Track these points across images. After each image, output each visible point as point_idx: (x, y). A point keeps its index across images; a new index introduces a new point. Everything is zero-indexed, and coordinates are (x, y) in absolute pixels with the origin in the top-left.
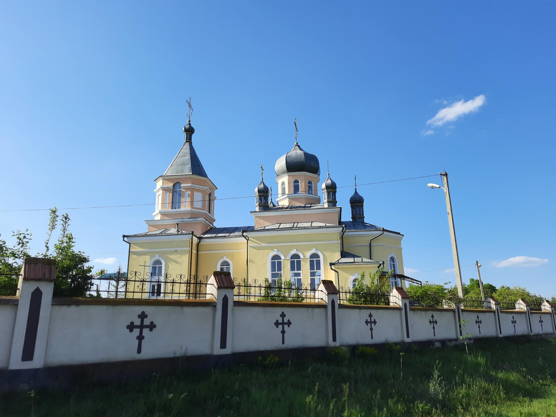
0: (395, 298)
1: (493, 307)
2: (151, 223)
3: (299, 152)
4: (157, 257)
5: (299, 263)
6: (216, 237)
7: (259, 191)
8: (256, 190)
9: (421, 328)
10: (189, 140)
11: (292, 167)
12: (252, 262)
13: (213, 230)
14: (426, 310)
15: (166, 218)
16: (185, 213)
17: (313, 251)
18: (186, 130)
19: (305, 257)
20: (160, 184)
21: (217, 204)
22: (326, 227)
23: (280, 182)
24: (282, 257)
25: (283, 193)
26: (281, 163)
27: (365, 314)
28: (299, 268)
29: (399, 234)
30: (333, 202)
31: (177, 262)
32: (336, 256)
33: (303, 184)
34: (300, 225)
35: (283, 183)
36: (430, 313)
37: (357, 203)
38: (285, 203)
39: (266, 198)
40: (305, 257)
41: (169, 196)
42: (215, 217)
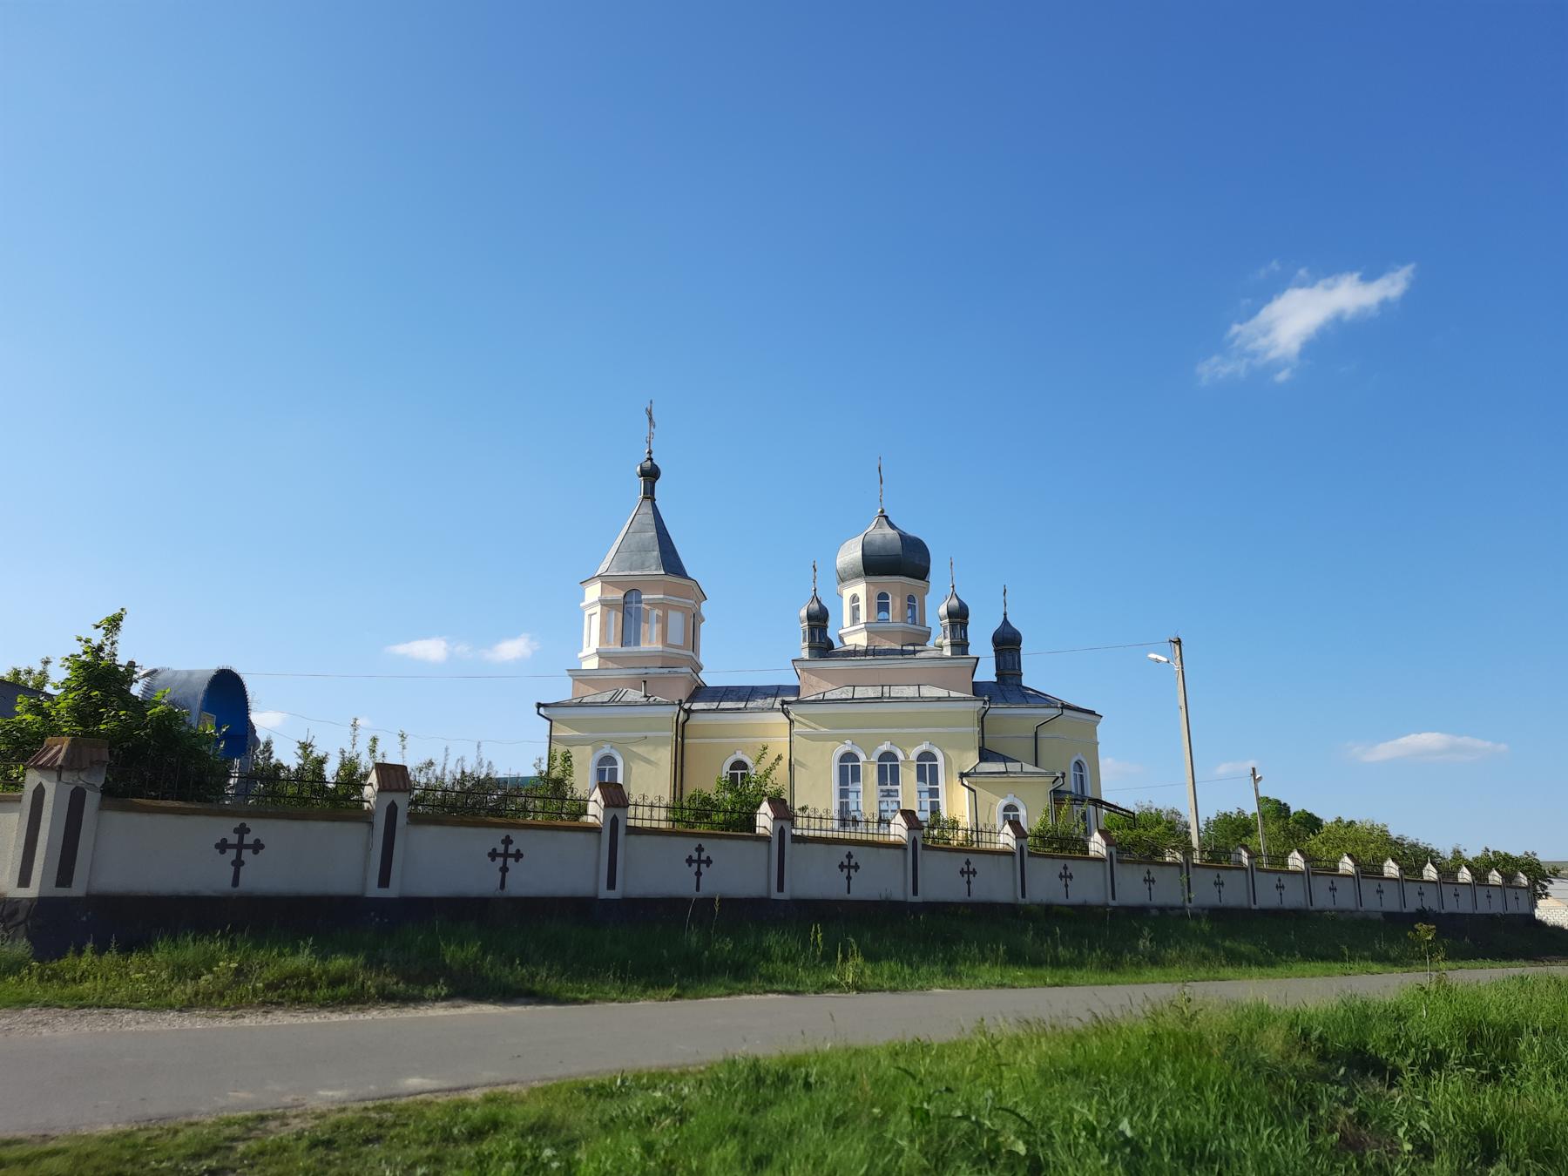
0: (1097, 845)
1: (1245, 861)
2: (579, 676)
3: (889, 531)
4: (606, 750)
5: (895, 769)
6: (717, 710)
7: (810, 617)
8: (804, 613)
9: (1132, 888)
10: (649, 494)
11: (875, 565)
12: (802, 765)
13: (700, 692)
14: (1140, 863)
15: (610, 665)
16: (651, 656)
17: (924, 747)
18: (644, 473)
19: (908, 757)
20: (594, 592)
21: (704, 629)
22: (949, 699)
23: (847, 593)
24: (862, 757)
25: (855, 618)
26: (851, 554)
27: (1058, 865)
28: (895, 781)
29: (1092, 713)
30: (961, 646)
31: (648, 761)
32: (971, 760)
33: (898, 601)
34: (896, 692)
35: (855, 598)
36: (1144, 868)
37: (1007, 643)
38: (858, 640)
39: (824, 629)
40: (908, 757)
41: (616, 618)
42: (703, 660)
